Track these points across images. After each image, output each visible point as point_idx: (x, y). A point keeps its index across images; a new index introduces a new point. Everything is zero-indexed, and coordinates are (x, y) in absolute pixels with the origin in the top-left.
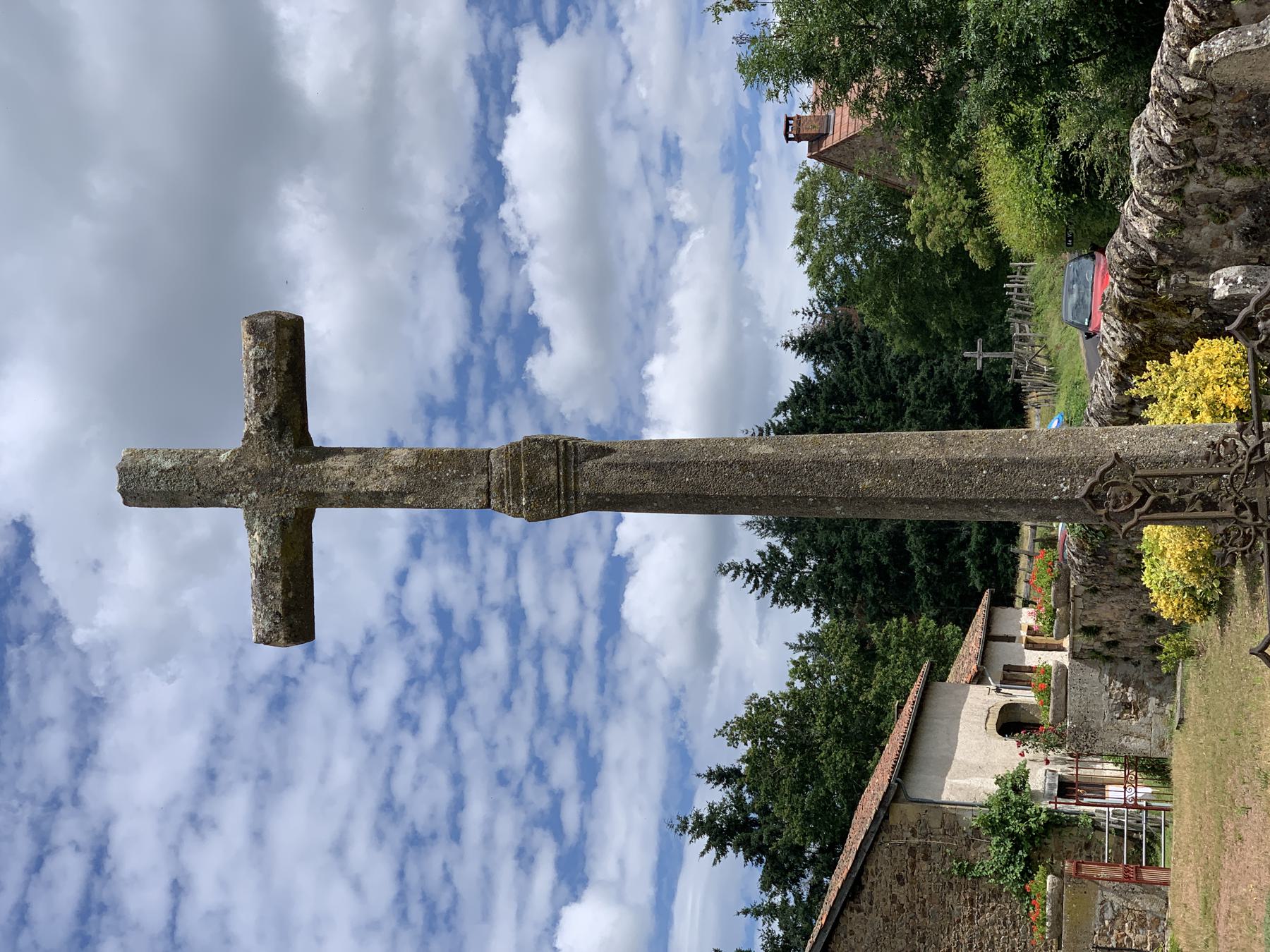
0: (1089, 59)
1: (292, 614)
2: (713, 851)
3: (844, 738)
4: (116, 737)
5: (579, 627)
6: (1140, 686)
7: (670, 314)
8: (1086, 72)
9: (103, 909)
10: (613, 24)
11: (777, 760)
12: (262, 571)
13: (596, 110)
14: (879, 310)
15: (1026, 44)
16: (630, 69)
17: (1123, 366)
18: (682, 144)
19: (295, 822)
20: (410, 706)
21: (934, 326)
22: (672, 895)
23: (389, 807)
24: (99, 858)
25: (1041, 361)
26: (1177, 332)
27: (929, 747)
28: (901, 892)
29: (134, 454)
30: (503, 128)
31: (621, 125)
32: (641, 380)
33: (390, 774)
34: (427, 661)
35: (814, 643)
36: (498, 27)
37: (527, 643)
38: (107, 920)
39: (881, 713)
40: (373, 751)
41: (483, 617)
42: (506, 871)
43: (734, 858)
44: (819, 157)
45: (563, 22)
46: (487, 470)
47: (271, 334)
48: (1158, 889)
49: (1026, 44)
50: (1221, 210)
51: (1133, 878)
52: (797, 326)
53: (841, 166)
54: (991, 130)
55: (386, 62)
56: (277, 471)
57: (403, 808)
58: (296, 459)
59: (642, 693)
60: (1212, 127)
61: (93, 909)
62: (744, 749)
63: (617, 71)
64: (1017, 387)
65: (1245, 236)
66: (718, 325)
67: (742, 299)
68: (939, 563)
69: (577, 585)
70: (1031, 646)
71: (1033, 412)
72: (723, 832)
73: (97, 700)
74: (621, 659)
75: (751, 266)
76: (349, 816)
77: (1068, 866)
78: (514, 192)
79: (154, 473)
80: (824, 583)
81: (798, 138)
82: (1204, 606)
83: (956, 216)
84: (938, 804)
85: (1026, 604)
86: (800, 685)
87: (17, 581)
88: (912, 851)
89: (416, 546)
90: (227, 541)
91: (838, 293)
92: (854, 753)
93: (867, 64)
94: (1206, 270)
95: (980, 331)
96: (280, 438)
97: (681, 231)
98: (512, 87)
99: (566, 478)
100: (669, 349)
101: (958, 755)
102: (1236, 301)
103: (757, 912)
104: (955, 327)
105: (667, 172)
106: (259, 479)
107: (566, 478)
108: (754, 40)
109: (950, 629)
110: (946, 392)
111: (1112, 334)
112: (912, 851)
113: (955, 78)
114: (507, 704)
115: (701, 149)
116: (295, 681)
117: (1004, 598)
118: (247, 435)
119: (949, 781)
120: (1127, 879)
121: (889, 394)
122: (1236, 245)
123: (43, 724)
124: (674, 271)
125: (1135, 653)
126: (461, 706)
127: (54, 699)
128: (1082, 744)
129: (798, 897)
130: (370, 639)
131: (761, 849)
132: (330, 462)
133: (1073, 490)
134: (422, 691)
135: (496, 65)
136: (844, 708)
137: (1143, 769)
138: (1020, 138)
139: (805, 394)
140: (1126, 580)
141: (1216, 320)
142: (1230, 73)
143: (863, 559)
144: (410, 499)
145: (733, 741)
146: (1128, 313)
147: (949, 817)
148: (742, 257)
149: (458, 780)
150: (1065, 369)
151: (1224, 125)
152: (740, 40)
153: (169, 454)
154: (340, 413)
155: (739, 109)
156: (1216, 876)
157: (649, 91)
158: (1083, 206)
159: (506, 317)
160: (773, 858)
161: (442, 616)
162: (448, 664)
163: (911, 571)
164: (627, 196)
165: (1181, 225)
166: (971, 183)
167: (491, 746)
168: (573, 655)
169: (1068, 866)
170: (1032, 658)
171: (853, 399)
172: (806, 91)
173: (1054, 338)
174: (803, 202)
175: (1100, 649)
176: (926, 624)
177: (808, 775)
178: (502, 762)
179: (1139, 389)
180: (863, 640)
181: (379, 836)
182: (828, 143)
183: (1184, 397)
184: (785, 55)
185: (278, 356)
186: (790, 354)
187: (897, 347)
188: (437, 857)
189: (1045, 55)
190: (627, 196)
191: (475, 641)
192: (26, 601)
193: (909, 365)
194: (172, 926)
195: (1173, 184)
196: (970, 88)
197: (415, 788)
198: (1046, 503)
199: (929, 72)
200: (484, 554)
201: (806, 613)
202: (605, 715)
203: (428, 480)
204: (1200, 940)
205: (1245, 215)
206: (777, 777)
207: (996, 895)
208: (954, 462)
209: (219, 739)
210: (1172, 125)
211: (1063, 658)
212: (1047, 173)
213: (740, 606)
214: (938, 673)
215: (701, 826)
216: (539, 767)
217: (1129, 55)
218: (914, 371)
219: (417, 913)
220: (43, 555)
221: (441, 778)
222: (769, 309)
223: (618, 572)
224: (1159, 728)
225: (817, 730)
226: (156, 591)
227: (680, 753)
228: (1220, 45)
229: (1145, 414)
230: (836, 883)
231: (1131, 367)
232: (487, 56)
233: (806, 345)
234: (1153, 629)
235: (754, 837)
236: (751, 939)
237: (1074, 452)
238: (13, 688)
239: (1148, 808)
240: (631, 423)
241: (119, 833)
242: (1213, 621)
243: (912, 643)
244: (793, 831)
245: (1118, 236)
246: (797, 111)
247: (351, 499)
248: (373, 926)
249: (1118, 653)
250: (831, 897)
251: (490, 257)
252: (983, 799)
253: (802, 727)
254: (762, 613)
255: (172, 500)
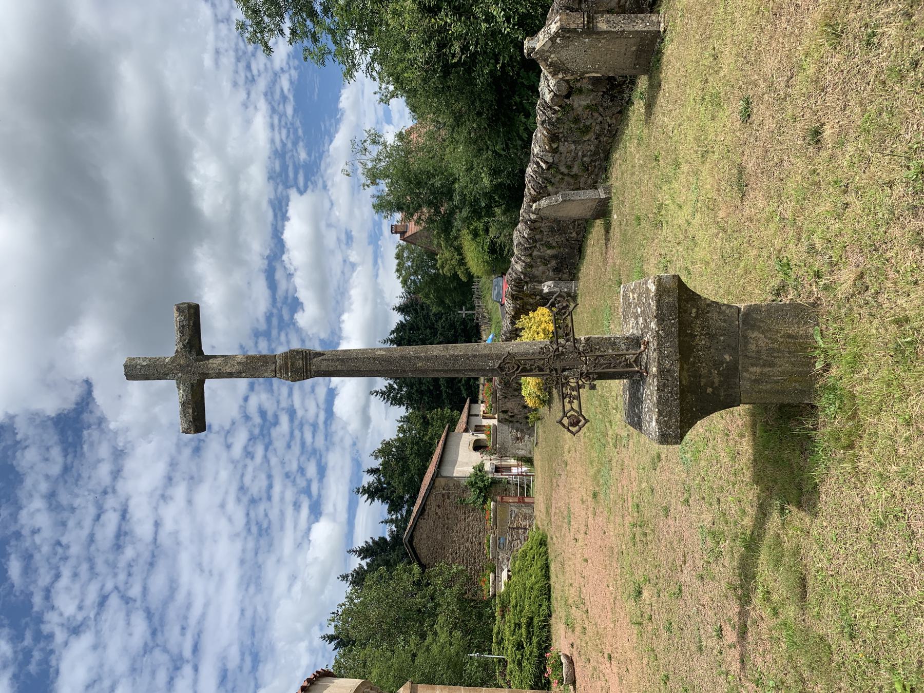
0: (499, 206)
1: (196, 418)
2: (370, 500)
3: (418, 455)
4: (130, 465)
5: (317, 416)
6: (522, 431)
7: (350, 298)
8: (498, 211)
9: (126, 533)
10: (325, 187)
11: (393, 464)
12: (184, 405)
13: (320, 220)
14: (427, 296)
15: (477, 201)
16: (332, 204)
17: (513, 317)
18: (353, 233)
19: (204, 496)
20: (250, 449)
21: (447, 301)
22: (354, 517)
23: (242, 489)
24: (124, 514)
25: (486, 314)
26: (531, 305)
27: (449, 457)
28: (439, 512)
29: (131, 360)
30: (283, 226)
31: (329, 225)
32: (339, 322)
33: (242, 476)
34: (257, 431)
35: (406, 419)
36: (281, 187)
37: (297, 422)
38: (128, 538)
39: (431, 444)
40: (235, 467)
41: (279, 413)
42: (289, 511)
43: (377, 502)
44: (404, 240)
45: (306, 187)
46: (275, 363)
47: (186, 311)
48: (530, 505)
49: (477, 201)
50: (545, 261)
51: (521, 501)
52: (398, 302)
53: (412, 243)
54: (465, 231)
55: (237, 200)
56: (189, 365)
57: (248, 489)
58: (197, 360)
59: (342, 440)
60: (541, 231)
61: (122, 536)
62: (381, 460)
63: (327, 204)
64: (477, 324)
65: (554, 270)
66: (366, 305)
67: (378, 292)
68: (451, 388)
69: (316, 399)
70: (484, 417)
71: (483, 333)
72: (373, 493)
73: (122, 451)
74: (334, 428)
75: (379, 280)
76: (226, 493)
77: (499, 498)
78: (288, 250)
79: (139, 367)
80: (409, 396)
81: (396, 233)
82: (543, 402)
83: (454, 262)
84: (452, 478)
85: (482, 402)
86: (401, 435)
87: (88, 404)
88: (443, 496)
89: (252, 387)
90: (168, 396)
91: (412, 290)
92: (422, 460)
93: (420, 206)
94: (541, 282)
95: (464, 303)
96: (190, 352)
97: (353, 266)
98: (287, 211)
99: (304, 365)
100: (350, 310)
101: (459, 459)
102: (551, 294)
103: (386, 522)
104: (455, 302)
105: (347, 244)
106: (182, 368)
107: (304, 365)
108: (378, 197)
109: (455, 413)
110: (452, 326)
111: (509, 305)
112: (443, 496)
113: (452, 213)
114: (289, 446)
115: (361, 235)
116: (203, 441)
117: (475, 401)
118: (177, 351)
119: (456, 469)
120: (519, 502)
121: (432, 327)
122: (551, 274)
123: (99, 461)
124: (351, 281)
125: (520, 419)
126: (271, 448)
127: (104, 451)
128: (502, 453)
129: (402, 515)
130: (233, 423)
131: (388, 498)
132: (211, 361)
133: (494, 365)
134: (254, 443)
135: (280, 202)
136: (418, 443)
137: (524, 461)
138: (475, 234)
139: (401, 327)
140: (516, 393)
141: (544, 300)
142: (546, 213)
143: (424, 388)
144: (244, 375)
145: (377, 457)
146: (514, 298)
147: (456, 482)
148: (377, 276)
149: (270, 477)
150: (494, 317)
151: (545, 230)
152: (373, 196)
153: (145, 359)
154: (217, 340)
155: (374, 221)
156: (550, 499)
157: (340, 214)
158: (498, 258)
159: (286, 298)
160: (392, 501)
161: (263, 413)
162: (265, 432)
163: (441, 392)
164: (332, 252)
165: (532, 266)
166: (459, 250)
167: (283, 463)
168: (315, 426)
169: (499, 498)
170: (485, 422)
171: (419, 329)
172: (398, 216)
173: (490, 306)
174: (399, 256)
175: (508, 418)
176: (447, 411)
177: (405, 469)
178: (287, 469)
179: (519, 325)
180: (424, 417)
181: (239, 500)
182: (407, 235)
183: (534, 328)
184: (390, 203)
185: (189, 320)
186: (395, 312)
187: (434, 309)
188: (262, 507)
189: (483, 205)
190: (332, 252)
191: (276, 423)
192: (91, 412)
193: (439, 316)
194: (155, 539)
195: (529, 252)
196: (457, 216)
197: (253, 481)
198: (484, 370)
199: (442, 210)
200: (279, 389)
201: (403, 408)
202: (327, 449)
203: (252, 367)
204: (545, 523)
205: (553, 263)
206: (393, 471)
207: (474, 510)
208: (451, 356)
209: (173, 464)
210: (528, 231)
211: (495, 422)
212: (486, 247)
213: (378, 406)
214: (452, 429)
215: (365, 491)
216: (302, 470)
217: (513, 205)
218: (441, 318)
219: (254, 529)
220: (96, 394)
221: (263, 476)
222: (387, 295)
223: (332, 394)
224: (529, 446)
225: (408, 452)
226: (143, 412)
227: (357, 463)
228: (544, 202)
229: (521, 334)
230: (415, 509)
231: (515, 317)
232: (277, 198)
233: (401, 309)
234: (526, 410)
235: (385, 494)
236: (384, 532)
237: (494, 351)
238: (85, 447)
239: (526, 475)
240: (336, 338)
241: (132, 504)
242: (546, 407)
243: (442, 418)
244: (400, 491)
245: (510, 270)
246: (395, 223)
247: (220, 375)
248: (237, 535)
249: (514, 419)
250: (414, 515)
251: (279, 275)
252: (468, 475)
253: (402, 451)
254: (386, 407)
255: (147, 378)
